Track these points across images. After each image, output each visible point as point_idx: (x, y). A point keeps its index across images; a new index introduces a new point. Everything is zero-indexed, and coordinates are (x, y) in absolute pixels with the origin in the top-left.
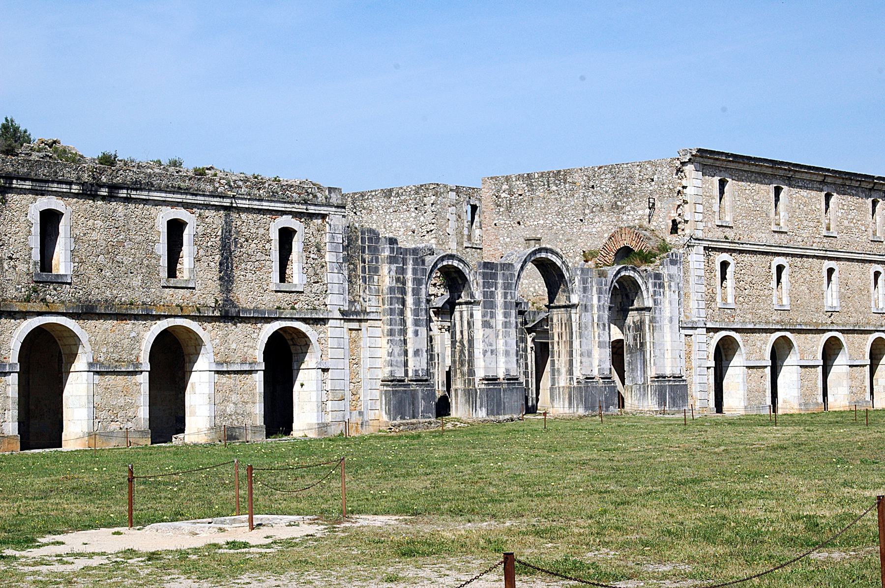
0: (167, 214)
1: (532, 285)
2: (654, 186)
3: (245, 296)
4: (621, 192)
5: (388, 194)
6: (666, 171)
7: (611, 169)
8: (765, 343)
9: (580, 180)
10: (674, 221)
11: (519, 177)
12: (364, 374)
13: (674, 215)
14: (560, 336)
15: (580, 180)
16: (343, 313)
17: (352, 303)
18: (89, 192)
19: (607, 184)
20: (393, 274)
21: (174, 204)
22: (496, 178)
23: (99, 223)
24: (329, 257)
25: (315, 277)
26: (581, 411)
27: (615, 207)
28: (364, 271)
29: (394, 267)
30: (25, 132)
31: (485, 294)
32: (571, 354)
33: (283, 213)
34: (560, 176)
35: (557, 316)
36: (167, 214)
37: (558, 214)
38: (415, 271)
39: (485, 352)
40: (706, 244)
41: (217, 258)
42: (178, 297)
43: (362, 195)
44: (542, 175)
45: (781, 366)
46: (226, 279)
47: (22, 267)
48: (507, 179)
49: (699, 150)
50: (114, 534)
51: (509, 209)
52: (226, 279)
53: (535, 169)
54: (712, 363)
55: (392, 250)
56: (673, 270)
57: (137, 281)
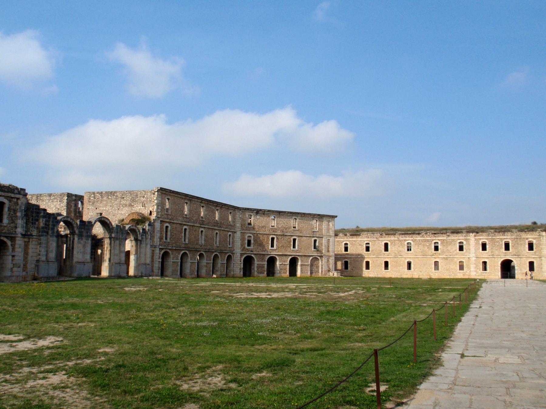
0: (313, 239)
2: (144, 199)
4: (133, 200)
5: (50, 195)
6: (149, 194)
7: (130, 192)
8: (179, 254)
9: (119, 195)
10: (151, 212)
11: (98, 193)
12: (29, 258)
14: (107, 248)
15: (119, 195)
17: (26, 231)
19: (129, 198)
20: (44, 222)
22: (89, 192)
24: (19, 214)
26: (271, 375)
27: (131, 205)
28: (32, 220)
29: (44, 220)
30: (418, 389)
31: (79, 232)
34: (112, 193)
36: (313, 239)
37: (111, 206)
38: (53, 222)
39: (78, 253)
40: (161, 219)
43: (41, 195)
44: (106, 192)
45: (186, 262)
48: (94, 193)
49: (161, 188)
51: (93, 203)
53: (104, 190)
55: (44, 213)
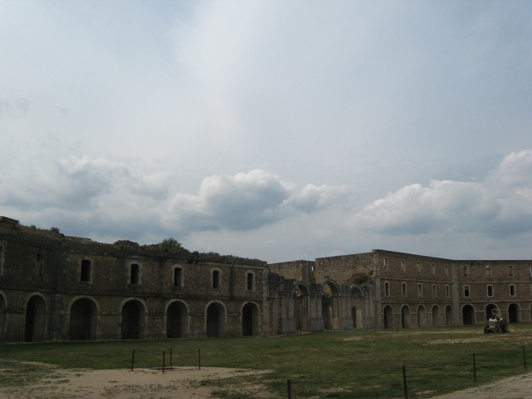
1: (327, 290)
3: (237, 293)
13: (371, 269)
16: (267, 298)
17: (270, 296)
18: (190, 262)
21: (215, 267)
23: (192, 272)
24: (264, 282)
25: (259, 287)
27: (354, 267)
32: (338, 311)
33: (249, 269)
35: (335, 300)
40: (381, 277)
41: (229, 282)
42: (216, 294)
46: (231, 289)
47: (169, 285)
50: (77, 375)
51: (323, 268)
52: (231, 289)
54: (383, 314)
56: (371, 286)
57: (203, 289)
